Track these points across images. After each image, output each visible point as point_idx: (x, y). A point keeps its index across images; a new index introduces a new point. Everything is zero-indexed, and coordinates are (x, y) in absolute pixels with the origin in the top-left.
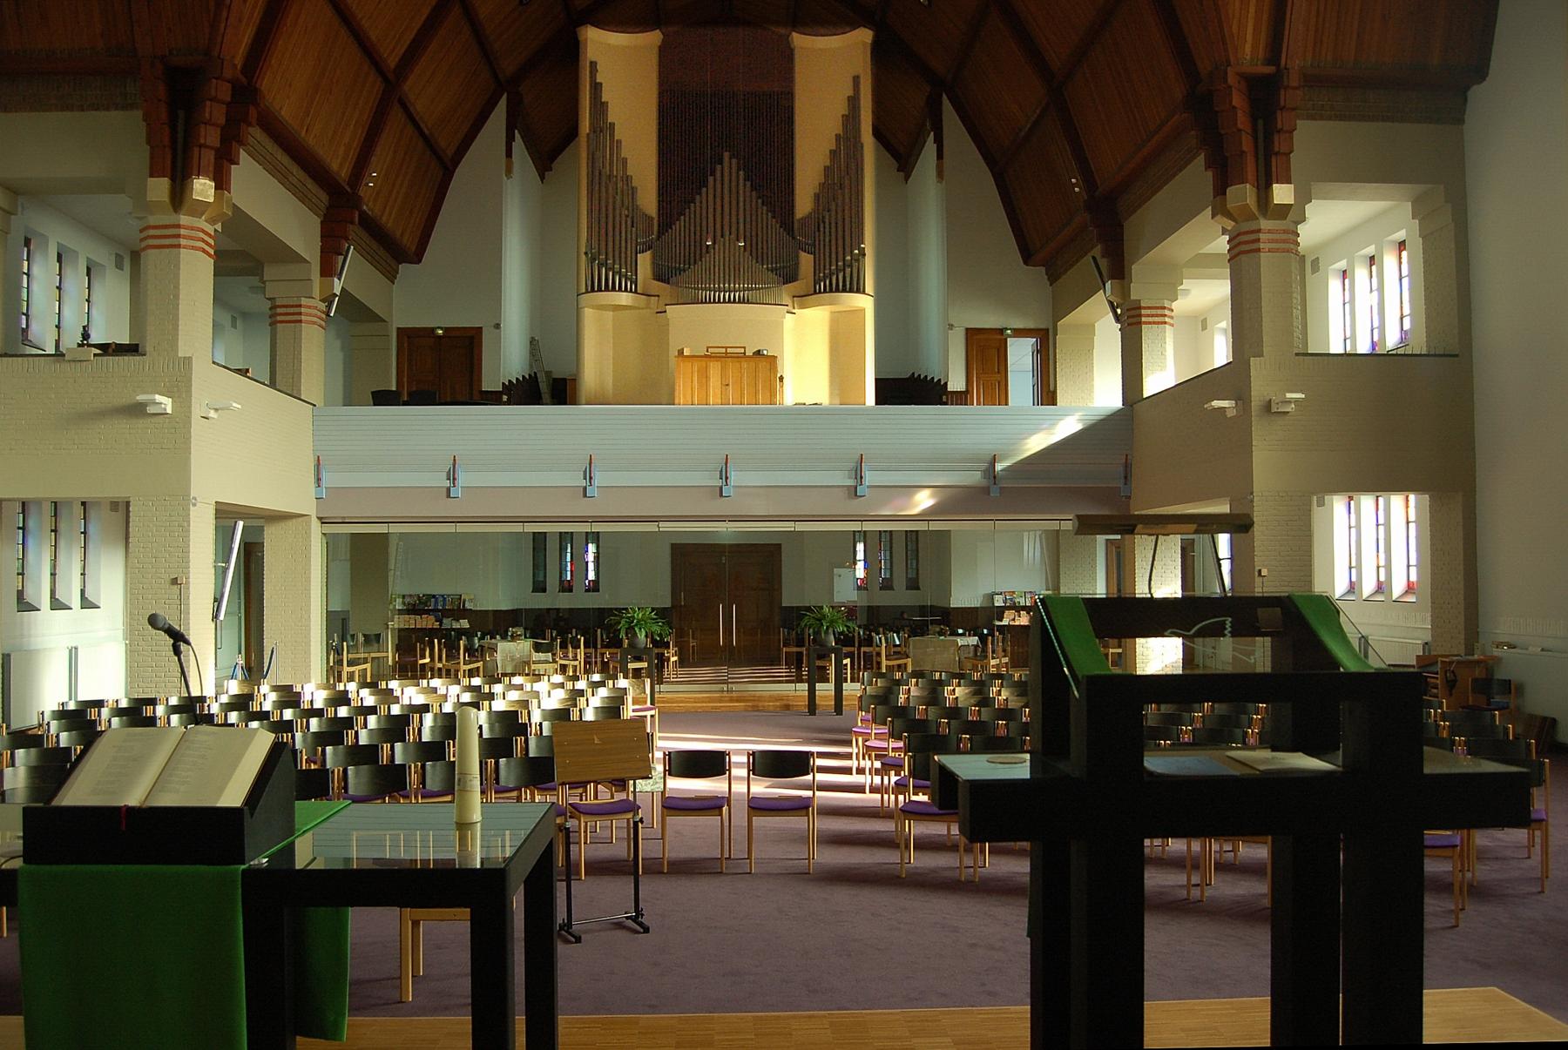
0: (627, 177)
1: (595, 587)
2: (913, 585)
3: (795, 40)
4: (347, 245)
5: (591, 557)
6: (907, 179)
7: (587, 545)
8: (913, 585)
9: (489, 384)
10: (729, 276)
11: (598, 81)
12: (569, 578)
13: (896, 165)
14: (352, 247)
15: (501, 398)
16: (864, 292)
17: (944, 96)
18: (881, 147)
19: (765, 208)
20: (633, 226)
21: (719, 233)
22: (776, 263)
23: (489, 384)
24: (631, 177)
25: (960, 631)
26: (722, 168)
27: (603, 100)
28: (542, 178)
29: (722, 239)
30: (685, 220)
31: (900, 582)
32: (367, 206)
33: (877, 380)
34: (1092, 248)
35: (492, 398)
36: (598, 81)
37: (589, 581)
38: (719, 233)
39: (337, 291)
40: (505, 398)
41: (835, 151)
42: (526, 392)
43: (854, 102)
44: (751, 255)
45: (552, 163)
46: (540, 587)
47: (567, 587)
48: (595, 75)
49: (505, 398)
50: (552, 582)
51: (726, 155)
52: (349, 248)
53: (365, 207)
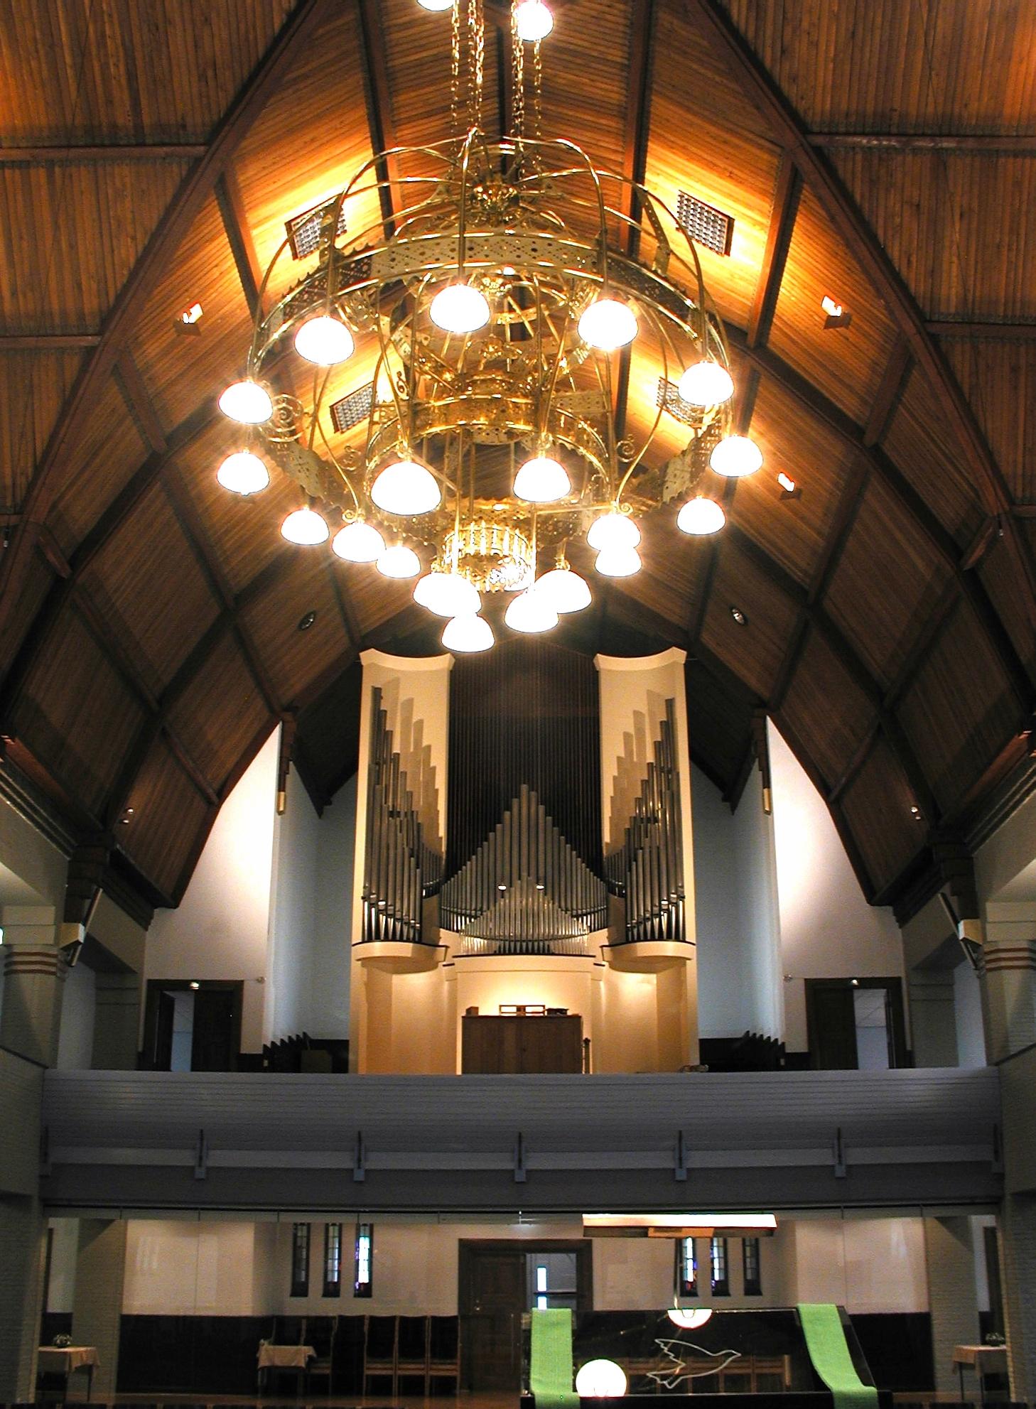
0: (413, 812)
1: (365, 1291)
2: (753, 1288)
3: (600, 661)
4: (95, 887)
5: (363, 1254)
6: (734, 808)
7: (358, 1241)
8: (753, 1288)
9: (249, 1045)
10: (572, 893)
11: (382, 708)
12: (336, 1280)
13: (720, 794)
14: (101, 890)
15: (262, 1063)
16: (684, 941)
17: (768, 718)
18: (700, 772)
19: (568, 846)
20: (417, 867)
21: (515, 875)
22: (582, 910)
23: (249, 1045)
24: (417, 812)
25: (195, 985)
26: (489, 845)
27: (387, 729)
28: (320, 813)
29: (519, 882)
30: (482, 853)
31: (736, 1285)
32: (121, 844)
33: (138, 1069)
34: (941, 887)
35: (251, 1063)
36: (382, 708)
37: (360, 1284)
38: (515, 875)
39: (81, 938)
40: (266, 1063)
41: (647, 781)
42: (996, 1137)
43: (668, 728)
44: (553, 899)
45: (331, 796)
46: (300, 1290)
47: (332, 1290)
48: (380, 702)
49: (266, 1063)
50: (316, 1286)
51: (524, 788)
52: (97, 892)
53: (118, 846)
